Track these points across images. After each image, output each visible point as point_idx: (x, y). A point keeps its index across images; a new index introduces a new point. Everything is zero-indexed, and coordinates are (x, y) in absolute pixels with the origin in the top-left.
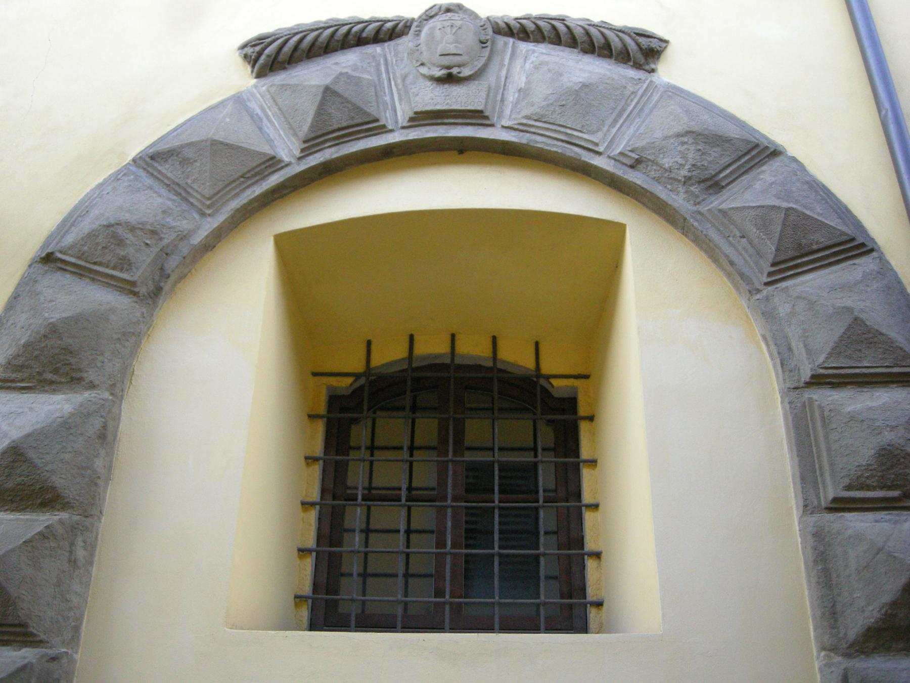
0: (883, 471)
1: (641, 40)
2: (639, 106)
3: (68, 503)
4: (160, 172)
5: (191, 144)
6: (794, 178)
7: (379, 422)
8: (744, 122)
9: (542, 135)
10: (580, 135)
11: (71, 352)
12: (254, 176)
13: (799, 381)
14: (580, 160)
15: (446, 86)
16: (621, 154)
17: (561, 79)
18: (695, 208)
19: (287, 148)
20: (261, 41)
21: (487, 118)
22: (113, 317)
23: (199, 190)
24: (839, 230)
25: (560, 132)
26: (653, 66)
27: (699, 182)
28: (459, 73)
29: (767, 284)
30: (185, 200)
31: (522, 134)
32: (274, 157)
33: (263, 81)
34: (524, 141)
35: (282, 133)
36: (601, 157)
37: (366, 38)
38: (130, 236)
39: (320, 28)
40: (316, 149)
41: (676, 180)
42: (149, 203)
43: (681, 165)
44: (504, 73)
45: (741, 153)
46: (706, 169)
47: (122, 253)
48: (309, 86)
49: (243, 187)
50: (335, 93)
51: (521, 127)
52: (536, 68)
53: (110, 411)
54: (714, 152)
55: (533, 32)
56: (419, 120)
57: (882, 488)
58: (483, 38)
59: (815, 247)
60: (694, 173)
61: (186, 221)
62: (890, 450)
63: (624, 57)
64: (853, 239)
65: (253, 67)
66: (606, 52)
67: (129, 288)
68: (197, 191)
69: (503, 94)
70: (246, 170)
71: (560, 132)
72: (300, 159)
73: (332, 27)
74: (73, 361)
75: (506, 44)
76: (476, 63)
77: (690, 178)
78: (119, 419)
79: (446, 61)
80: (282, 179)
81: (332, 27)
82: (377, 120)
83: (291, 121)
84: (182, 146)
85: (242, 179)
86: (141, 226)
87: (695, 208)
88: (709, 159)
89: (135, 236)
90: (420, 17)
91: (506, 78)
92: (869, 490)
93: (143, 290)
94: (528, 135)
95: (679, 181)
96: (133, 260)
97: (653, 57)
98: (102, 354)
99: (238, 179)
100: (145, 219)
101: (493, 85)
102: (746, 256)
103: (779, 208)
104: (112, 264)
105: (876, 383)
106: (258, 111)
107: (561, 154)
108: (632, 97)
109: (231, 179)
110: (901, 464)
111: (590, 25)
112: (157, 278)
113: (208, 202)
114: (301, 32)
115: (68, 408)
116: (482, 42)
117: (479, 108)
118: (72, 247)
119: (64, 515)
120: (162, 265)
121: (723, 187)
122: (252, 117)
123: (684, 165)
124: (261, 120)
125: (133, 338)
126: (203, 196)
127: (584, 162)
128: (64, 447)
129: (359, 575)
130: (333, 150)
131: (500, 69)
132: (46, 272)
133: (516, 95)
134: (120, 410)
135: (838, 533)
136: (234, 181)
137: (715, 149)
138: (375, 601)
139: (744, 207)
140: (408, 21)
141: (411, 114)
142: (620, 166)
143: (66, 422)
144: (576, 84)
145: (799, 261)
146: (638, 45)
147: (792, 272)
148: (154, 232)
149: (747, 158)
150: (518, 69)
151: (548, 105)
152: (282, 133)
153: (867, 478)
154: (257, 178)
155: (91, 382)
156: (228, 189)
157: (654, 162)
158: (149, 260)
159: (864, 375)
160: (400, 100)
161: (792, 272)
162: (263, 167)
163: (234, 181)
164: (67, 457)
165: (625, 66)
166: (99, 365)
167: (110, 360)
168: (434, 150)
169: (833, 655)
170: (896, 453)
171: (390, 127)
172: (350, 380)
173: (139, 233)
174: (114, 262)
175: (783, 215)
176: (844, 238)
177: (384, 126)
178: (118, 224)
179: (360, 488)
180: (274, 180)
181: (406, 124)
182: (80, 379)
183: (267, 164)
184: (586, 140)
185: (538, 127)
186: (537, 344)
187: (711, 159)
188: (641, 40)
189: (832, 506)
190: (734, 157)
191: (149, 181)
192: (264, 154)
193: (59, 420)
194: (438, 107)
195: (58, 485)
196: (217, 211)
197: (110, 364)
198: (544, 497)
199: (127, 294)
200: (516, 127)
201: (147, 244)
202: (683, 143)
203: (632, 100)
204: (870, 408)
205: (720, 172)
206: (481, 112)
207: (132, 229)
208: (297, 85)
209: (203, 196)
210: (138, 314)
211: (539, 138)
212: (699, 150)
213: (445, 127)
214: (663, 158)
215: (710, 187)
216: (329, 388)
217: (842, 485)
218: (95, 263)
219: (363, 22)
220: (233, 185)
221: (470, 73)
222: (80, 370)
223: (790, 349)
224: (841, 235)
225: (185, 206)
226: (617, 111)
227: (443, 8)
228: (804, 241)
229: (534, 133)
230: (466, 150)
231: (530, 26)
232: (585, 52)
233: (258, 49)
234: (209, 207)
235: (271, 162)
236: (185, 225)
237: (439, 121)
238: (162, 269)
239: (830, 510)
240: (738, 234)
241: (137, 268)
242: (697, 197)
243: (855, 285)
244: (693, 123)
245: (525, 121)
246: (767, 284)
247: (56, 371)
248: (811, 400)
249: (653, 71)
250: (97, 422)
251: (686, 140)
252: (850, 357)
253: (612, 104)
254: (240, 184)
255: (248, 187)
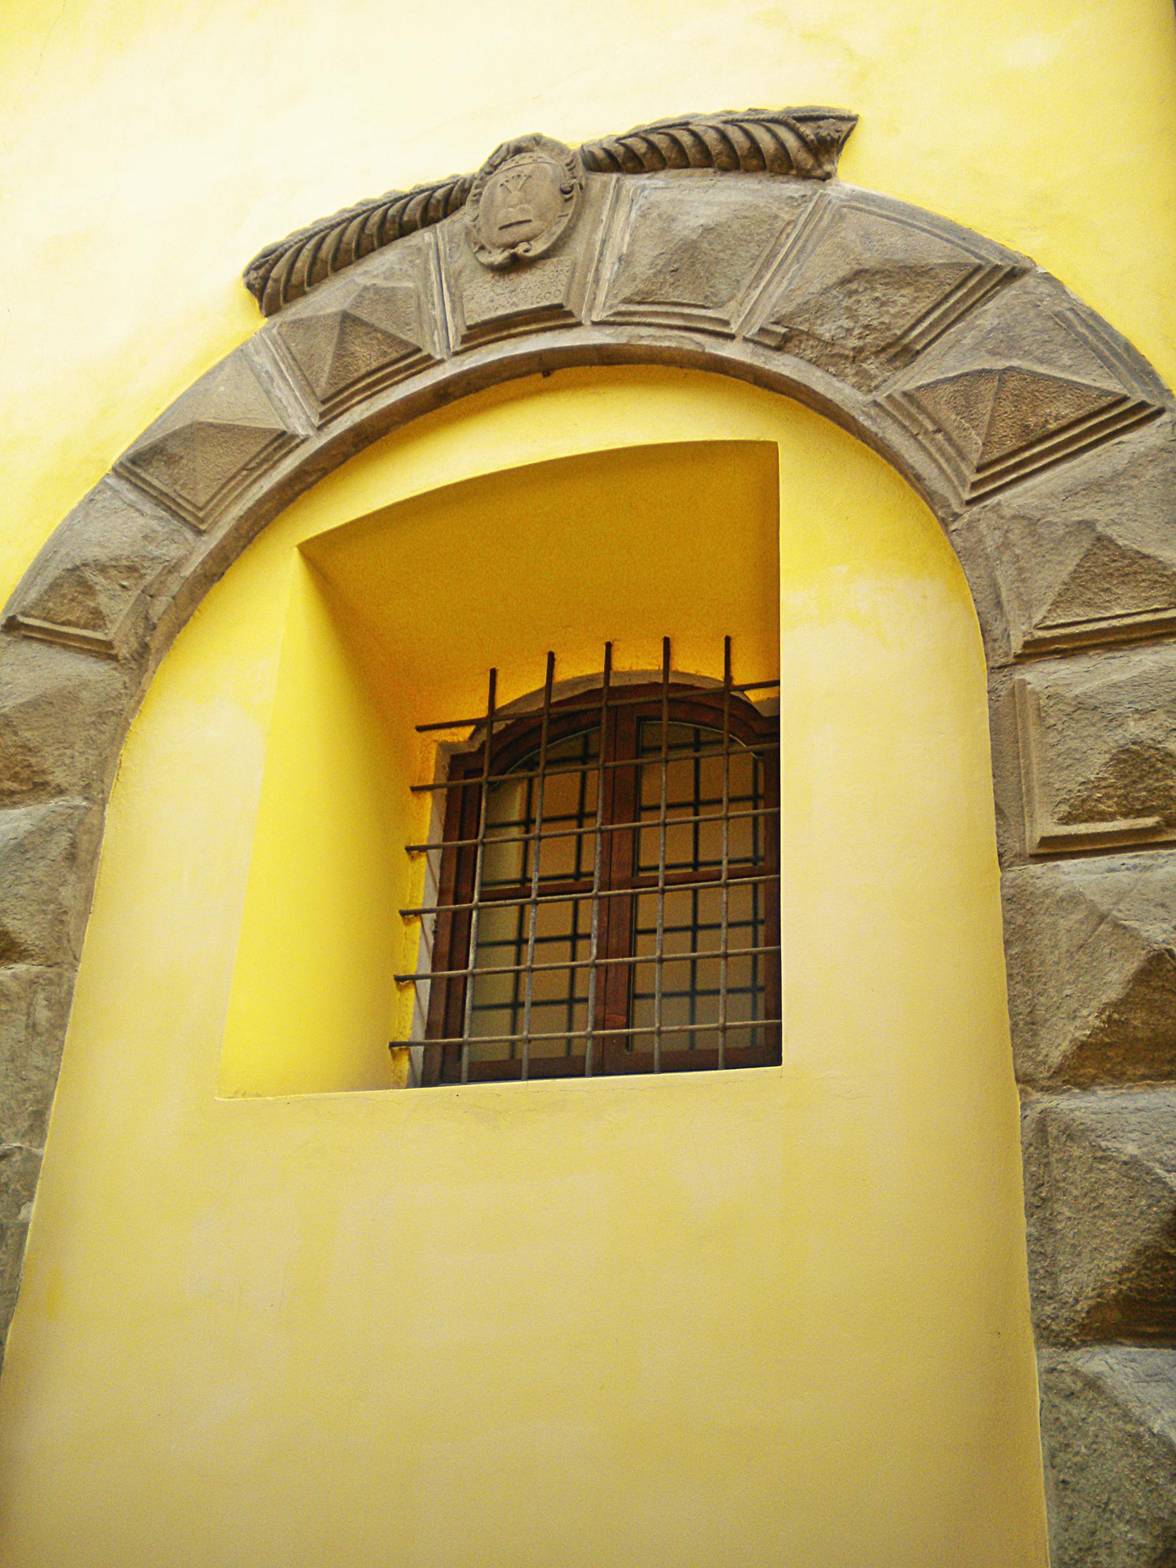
0: (1126, 786)
1: (807, 130)
2: (800, 243)
3: (25, 950)
4: (144, 481)
5: (174, 435)
6: (1032, 313)
7: (703, 763)
8: (969, 231)
9: (650, 325)
10: (702, 312)
11: (30, 750)
12: (260, 465)
13: (1007, 654)
14: (703, 353)
15: (513, 276)
16: (762, 331)
17: (674, 226)
18: (870, 398)
19: (298, 417)
20: (266, 262)
21: (570, 314)
22: (84, 694)
23: (189, 498)
24: (1097, 389)
25: (674, 315)
26: (828, 168)
27: (877, 354)
28: (527, 251)
29: (970, 503)
30: (174, 514)
31: (620, 329)
32: (284, 433)
33: (277, 319)
34: (623, 340)
35: (298, 394)
36: (735, 342)
37: (409, 221)
38: (100, 579)
39: (343, 221)
40: (341, 409)
41: (842, 356)
42: (131, 527)
43: (848, 330)
44: (600, 235)
45: (948, 289)
46: (888, 329)
47: (92, 604)
48: (324, 317)
49: (247, 482)
50: (357, 321)
51: (619, 319)
52: (643, 216)
53: (81, 822)
54: (902, 297)
55: (645, 154)
56: (476, 338)
57: (1125, 815)
58: (566, 187)
59: (1053, 426)
60: (869, 340)
61: (174, 545)
62: (1136, 752)
63: (780, 165)
64: (1125, 399)
65: (260, 300)
66: (755, 162)
67: (104, 651)
68: (188, 501)
69: (597, 270)
70: (247, 459)
71: (674, 315)
72: (320, 428)
73: (359, 215)
74: (33, 761)
75: (605, 186)
76: (554, 229)
77: (861, 350)
78: (101, 830)
79: (508, 236)
80: (297, 463)
81: (359, 215)
82: (419, 350)
83: (307, 373)
84: (165, 439)
85: (245, 473)
86: (113, 563)
87: (870, 398)
88: (892, 311)
89: (106, 578)
90: (482, 170)
91: (604, 242)
92: (1103, 820)
93: (123, 651)
94: (629, 328)
95: (847, 357)
96: (105, 611)
97: (828, 152)
98: (71, 747)
99: (239, 472)
100: (118, 552)
101: (580, 260)
102: (942, 461)
103: (990, 371)
104: (82, 622)
105: (1141, 639)
106: (269, 367)
107: (675, 349)
108: (789, 230)
109: (229, 474)
110: (1158, 771)
111: (726, 122)
112: (140, 631)
113: (201, 514)
114: (316, 234)
115: (25, 825)
116: (564, 192)
117: (556, 302)
118: (36, 604)
119: (20, 968)
120: (147, 612)
121: (918, 353)
122: (258, 377)
123: (853, 329)
124: (272, 379)
125: (113, 722)
126: (194, 506)
127: (710, 354)
128: (18, 878)
129: (523, 1005)
130: (363, 406)
131: (594, 230)
132: (9, 643)
133: (616, 267)
134: (103, 818)
135: (1046, 894)
136: (234, 477)
137: (904, 292)
138: (552, 1038)
139: (937, 382)
140: (465, 181)
141: (464, 331)
142: (760, 350)
143: (21, 845)
144: (694, 230)
145: (1027, 454)
146: (800, 137)
147: (1014, 476)
148: (132, 569)
149: (959, 294)
150: (621, 224)
151: (655, 275)
152: (298, 394)
153: (1099, 800)
154: (265, 467)
155: (58, 786)
156: (224, 491)
157: (809, 335)
158: (126, 608)
159: (1073, 637)
160: (453, 311)
161: (1014, 476)
162: (270, 449)
163: (234, 477)
164: (23, 890)
165: (785, 179)
166: (67, 762)
167: (82, 753)
168: (508, 379)
169: (1029, 1089)
170: (1147, 755)
171: (438, 357)
172: (469, 730)
173: (113, 572)
174: (86, 616)
175: (996, 383)
176: (1105, 401)
177: (429, 357)
178: (84, 565)
179: (725, 862)
180: (288, 465)
181: (459, 348)
182: (45, 784)
183: (276, 445)
184: (710, 319)
185: (643, 314)
186: (728, 640)
187: (897, 309)
188: (807, 130)
189: (1042, 851)
190: (935, 297)
191: (132, 496)
192: (271, 431)
193: (12, 842)
194: (501, 312)
195: (11, 929)
196: (215, 523)
197: (83, 759)
198: (729, 871)
199: (104, 660)
200: (612, 319)
201: (124, 587)
202: (850, 294)
203: (788, 236)
204: (1114, 685)
205: (913, 327)
206: (561, 306)
207: (102, 569)
208: (310, 319)
209: (194, 506)
210: (119, 686)
211: (645, 331)
212: (877, 298)
213: (513, 340)
214: (822, 325)
215: (896, 356)
216: (444, 746)
217: (1056, 816)
218: (63, 624)
219: (401, 198)
220: (233, 483)
221: (544, 247)
222: (44, 772)
223: (999, 604)
224: (1099, 397)
225: (176, 524)
226: (761, 261)
227: (511, 149)
228: (1032, 421)
229: (638, 324)
230: (553, 369)
231: (640, 147)
232: (725, 170)
233: (261, 272)
234: (202, 521)
235: (280, 441)
236: (173, 551)
237: (505, 333)
238: (146, 618)
239: (1038, 858)
240: (931, 427)
241: (111, 622)
242: (872, 378)
243: (1112, 479)
244: (867, 255)
245: (623, 308)
246: (970, 503)
247: (15, 777)
248: (1024, 683)
249: (828, 176)
250: (63, 840)
251: (854, 286)
252: (1089, 604)
253: (754, 250)
254: (243, 480)
255: (255, 481)
